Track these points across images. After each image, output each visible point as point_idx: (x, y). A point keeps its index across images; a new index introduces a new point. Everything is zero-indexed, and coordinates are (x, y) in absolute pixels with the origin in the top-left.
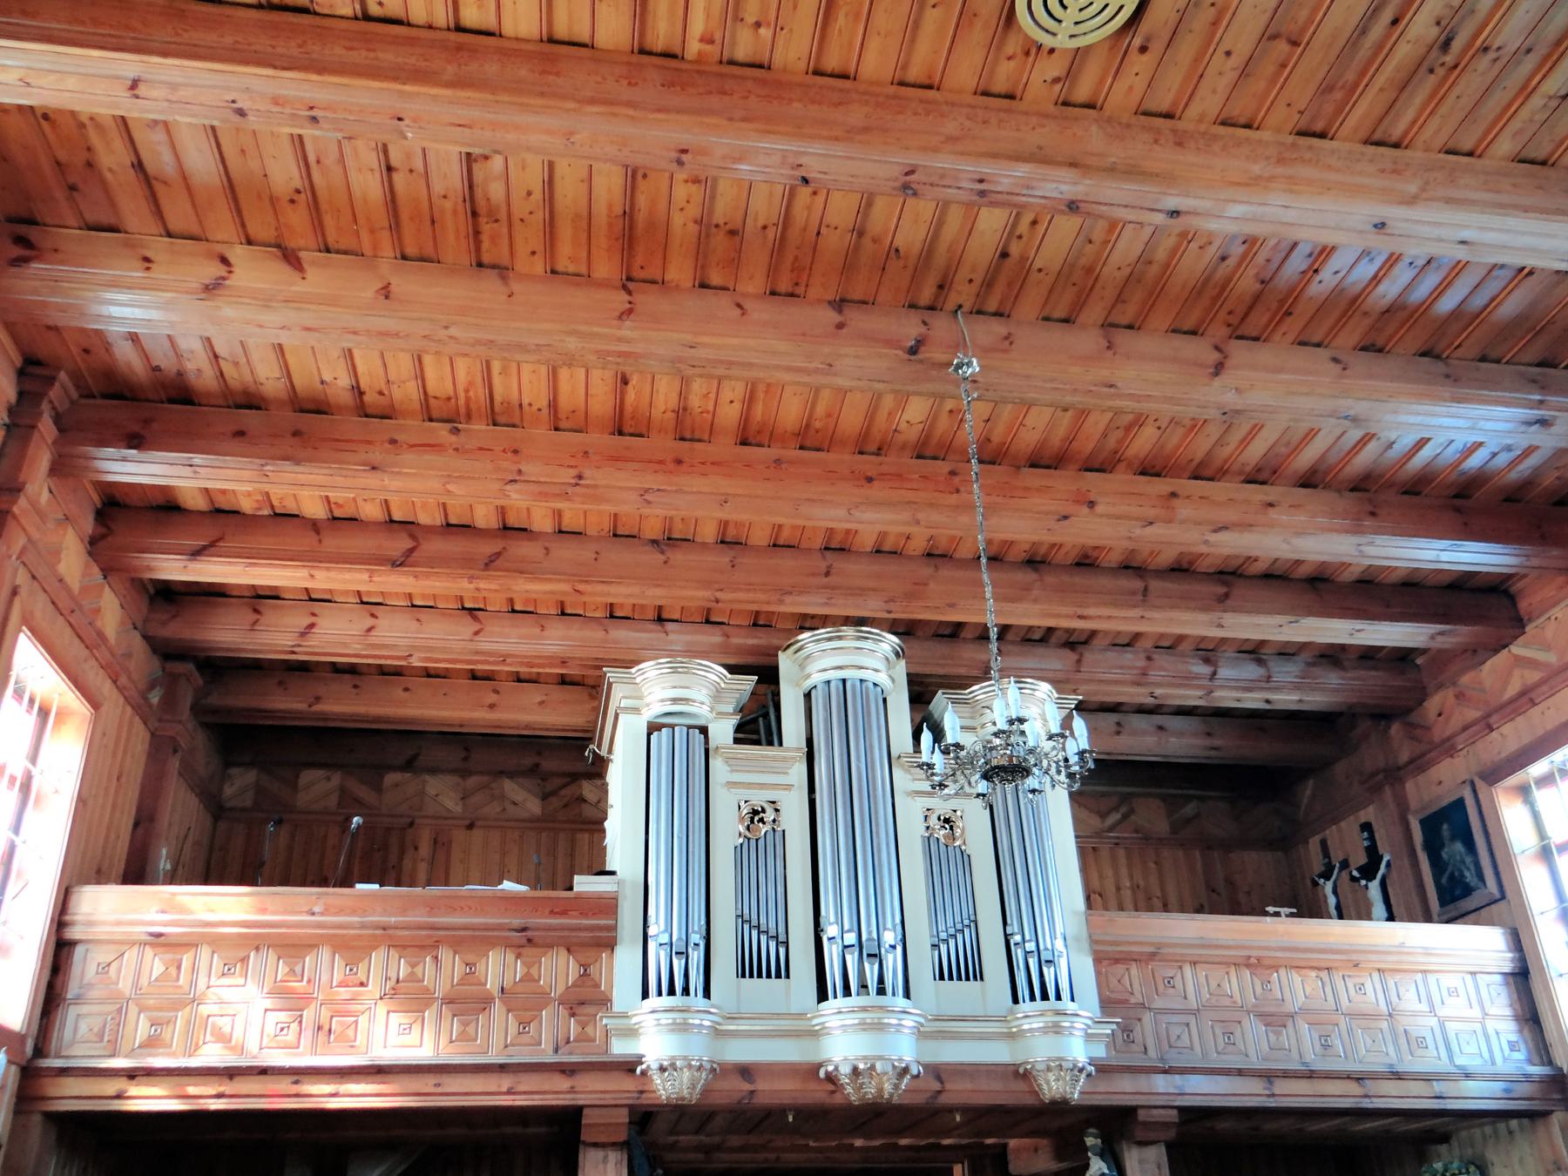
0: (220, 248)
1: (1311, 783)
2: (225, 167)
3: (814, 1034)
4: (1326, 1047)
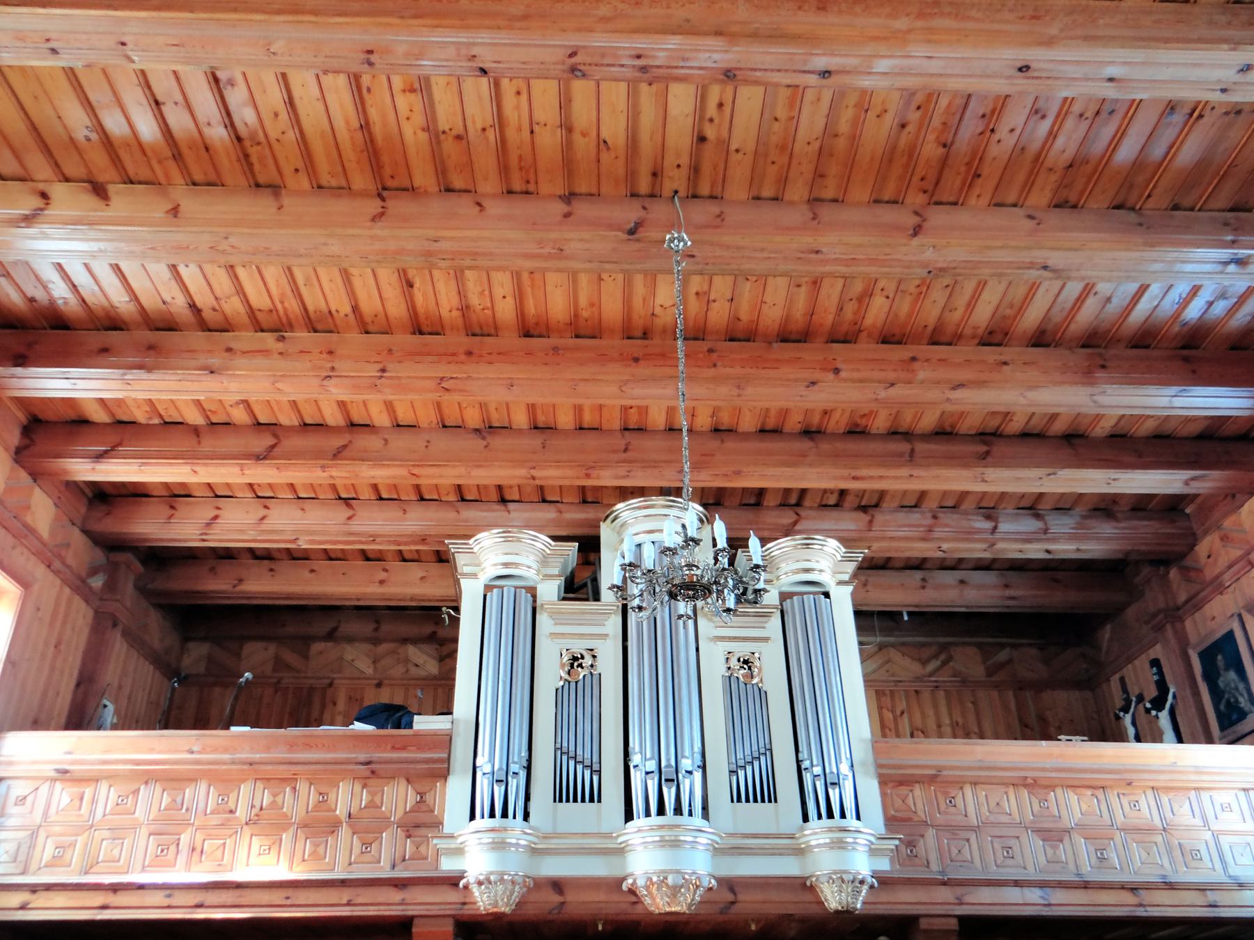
0: (41, 186)
1: (1108, 627)
2: (26, 114)
3: (621, 851)
4: (1102, 859)
